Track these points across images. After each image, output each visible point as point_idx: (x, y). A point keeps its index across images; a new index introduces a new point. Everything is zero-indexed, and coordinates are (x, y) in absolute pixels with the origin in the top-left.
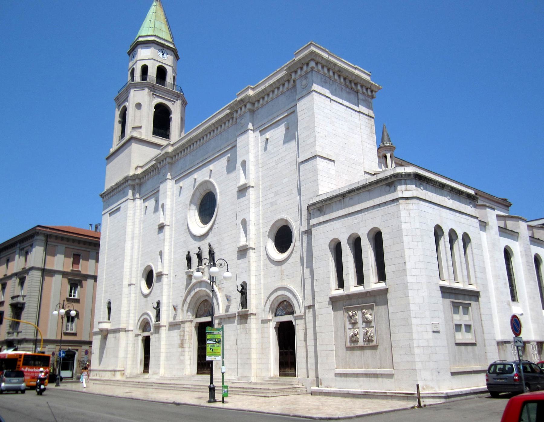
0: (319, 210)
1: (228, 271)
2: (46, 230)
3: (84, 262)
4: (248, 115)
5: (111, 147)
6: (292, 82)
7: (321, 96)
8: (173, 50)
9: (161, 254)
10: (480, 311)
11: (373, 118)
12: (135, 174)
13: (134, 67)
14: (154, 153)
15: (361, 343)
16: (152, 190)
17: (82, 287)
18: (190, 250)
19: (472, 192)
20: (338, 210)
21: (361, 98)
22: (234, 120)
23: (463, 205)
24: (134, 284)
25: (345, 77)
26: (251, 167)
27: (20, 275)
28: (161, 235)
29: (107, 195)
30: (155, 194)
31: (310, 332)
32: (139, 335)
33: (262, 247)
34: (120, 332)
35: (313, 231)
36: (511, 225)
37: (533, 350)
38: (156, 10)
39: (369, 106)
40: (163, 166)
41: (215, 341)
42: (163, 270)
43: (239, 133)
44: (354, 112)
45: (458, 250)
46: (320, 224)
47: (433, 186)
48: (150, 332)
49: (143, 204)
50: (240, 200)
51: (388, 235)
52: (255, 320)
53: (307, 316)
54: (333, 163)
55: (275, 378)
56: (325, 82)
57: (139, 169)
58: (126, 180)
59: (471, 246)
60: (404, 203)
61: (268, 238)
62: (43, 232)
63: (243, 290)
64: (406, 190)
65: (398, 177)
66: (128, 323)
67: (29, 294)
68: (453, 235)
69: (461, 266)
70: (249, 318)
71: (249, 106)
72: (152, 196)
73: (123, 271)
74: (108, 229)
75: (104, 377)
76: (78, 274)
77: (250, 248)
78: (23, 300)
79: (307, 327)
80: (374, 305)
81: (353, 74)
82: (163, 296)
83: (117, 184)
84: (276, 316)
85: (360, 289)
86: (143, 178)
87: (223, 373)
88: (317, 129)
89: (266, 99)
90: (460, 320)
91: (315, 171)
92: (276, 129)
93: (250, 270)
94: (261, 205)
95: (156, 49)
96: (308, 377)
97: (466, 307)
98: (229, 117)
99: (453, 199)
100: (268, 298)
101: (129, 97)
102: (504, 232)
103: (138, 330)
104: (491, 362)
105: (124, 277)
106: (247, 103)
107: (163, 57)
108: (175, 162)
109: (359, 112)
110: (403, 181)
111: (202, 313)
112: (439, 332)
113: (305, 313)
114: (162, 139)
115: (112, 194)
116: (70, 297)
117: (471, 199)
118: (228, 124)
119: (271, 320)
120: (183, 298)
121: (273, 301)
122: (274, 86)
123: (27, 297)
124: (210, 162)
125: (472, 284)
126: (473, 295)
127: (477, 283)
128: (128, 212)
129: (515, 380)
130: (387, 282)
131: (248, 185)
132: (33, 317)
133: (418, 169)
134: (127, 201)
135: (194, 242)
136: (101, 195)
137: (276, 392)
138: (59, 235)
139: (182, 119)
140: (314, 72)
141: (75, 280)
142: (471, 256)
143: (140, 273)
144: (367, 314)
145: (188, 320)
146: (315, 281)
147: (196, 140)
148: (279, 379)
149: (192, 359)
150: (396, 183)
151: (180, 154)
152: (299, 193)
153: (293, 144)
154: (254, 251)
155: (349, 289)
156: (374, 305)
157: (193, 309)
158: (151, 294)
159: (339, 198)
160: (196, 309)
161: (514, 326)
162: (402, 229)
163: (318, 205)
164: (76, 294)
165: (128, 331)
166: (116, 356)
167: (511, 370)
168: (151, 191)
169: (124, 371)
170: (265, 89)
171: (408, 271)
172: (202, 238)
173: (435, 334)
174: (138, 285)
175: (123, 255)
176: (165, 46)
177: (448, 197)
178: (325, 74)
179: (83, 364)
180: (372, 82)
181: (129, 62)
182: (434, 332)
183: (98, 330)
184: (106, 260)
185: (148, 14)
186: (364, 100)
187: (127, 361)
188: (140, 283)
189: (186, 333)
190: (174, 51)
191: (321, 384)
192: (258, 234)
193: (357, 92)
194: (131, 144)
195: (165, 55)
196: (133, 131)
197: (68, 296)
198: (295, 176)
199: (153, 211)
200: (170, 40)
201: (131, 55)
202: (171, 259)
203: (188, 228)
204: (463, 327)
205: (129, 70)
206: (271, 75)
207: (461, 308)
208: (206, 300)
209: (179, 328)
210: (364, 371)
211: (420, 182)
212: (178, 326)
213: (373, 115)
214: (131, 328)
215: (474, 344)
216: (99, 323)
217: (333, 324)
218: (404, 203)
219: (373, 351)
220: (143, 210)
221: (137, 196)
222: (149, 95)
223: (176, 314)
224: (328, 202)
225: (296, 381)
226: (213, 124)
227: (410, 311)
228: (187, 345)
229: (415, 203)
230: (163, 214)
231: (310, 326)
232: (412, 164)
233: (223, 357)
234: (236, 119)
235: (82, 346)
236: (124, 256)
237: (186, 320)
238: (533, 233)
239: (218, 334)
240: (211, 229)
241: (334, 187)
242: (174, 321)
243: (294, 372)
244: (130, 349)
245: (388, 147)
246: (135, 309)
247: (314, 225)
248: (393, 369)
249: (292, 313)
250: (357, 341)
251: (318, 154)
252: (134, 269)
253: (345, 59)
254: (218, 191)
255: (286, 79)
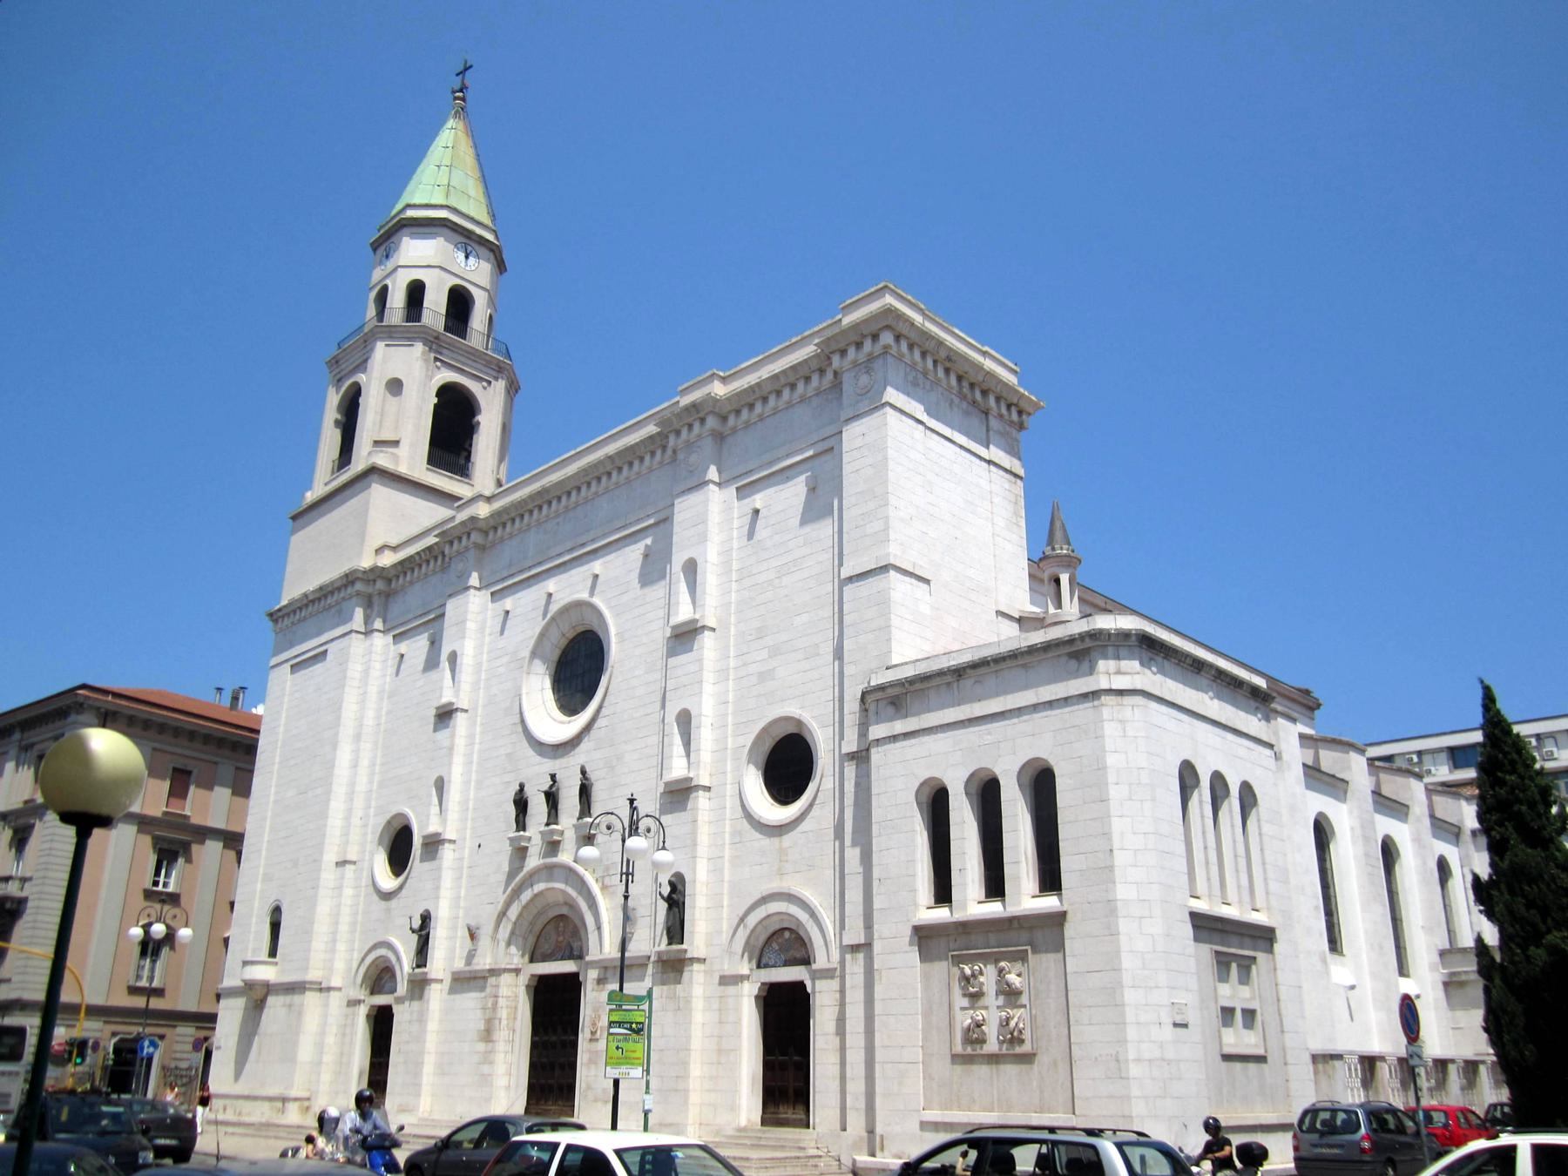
0: (893, 703)
1: (664, 848)
2: (105, 698)
3: (202, 792)
4: (708, 445)
5: (309, 487)
6: (829, 376)
7: (904, 418)
8: (494, 248)
9: (440, 785)
10: (1275, 977)
11: (1021, 478)
12: (377, 567)
13: (388, 282)
14: (430, 514)
15: (992, 1046)
16: (420, 613)
17: (189, 860)
18: (523, 781)
19: (1260, 682)
20: (942, 707)
21: (995, 428)
22: (669, 452)
23: (1242, 714)
24: (354, 863)
25: (960, 373)
26: (710, 579)
27: (17, 818)
28: (443, 735)
29: (288, 615)
30: (433, 622)
31: (855, 1013)
32: (359, 1002)
33: (729, 787)
34: (308, 993)
35: (876, 755)
36: (1329, 760)
37: (1351, 1076)
38: (455, 141)
39: (1013, 448)
40: (459, 553)
41: (631, 1029)
42: (444, 830)
43: (682, 487)
44: (978, 461)
45: (1229, 824)
46: (894, 738)
47: (1178, 664)
48: (396, 994)
49: (392, 648)
50: (673, 661)
51: (1070, 778)
52: (702, 974)
53: (847, 971)
54: (924, 586)
55: (752, 1130)
56: (915, 384)
57: (387, 552)
58: (350, 579)
59: (1258, 815)
60: (1111, 703)
61: (749, 763)
62: (98, 704)
63: (674, 896)
64: (1119, 672)
65: (1100, 640)
66: (330, 969)
67: (41, 874)
68: (1219, 784)
69: (1236, 863)
70: (686, 969)
71: (711, 422)
72: (421, 629)
73: (325, 825)
74: (285, 707)
75: (249, 1114)
76: (181, 823)
77: (697, 787)
78: (22, 889)
79: (847, 1000)
80: (1030, 952)
81: (979, 368)
82: (441, 900)
83: (321, 588)
84: (759, 967)
85: (994, 909)
86: (398, 577)
87: (646, 1113)
88: (892, 500)
89: (758, 408)
90: (1232, 997)
91: (883, 603)
92: (781, 487)
93: (695, 845)
94: (731, 677)
95: (449, 242)
96: (844, 1129)
97: (1246, 965)
98: (655, 444)
99: (1219, 697)
100: (742, 920)
101: (369, 361)
102: (1315, 778)
103: (358, 987)
104: (1306, 1103)
105: (327, 841)
106: (707, 414)
107: (466, 265)
108: (493, 545)
109: (989, 462)
110: (1110, 650)
111: (550, 951)
112: (1185, 1026)
113: (842, 962)
114: (451, 478)
115: (303, 614)
116: (155, 889)
117: (1259, 699)
118: (651, 462)
119: (747, 977)
120: (499, 907)
121: (755, 927)
122: (783, 381)
123: (34, 882)
124: (595, 553)
125: (1198, 895)
126: (1260, 937)
127: (1269, 909)
128: (350, 665)
129: (1363, 1151)
130: (1064, 896)
131: (700, 624)
132: (45, 938)
133: (1146, 622)
134: (347, 637)
135: (538, 758)
136: (271, 615)
137: (766, 1168)
138: (169, 722)
139: (505, 429)
140: (890, 359)
141: (171, 841)
142: (1258, 839)
143: (373, 833)
144: (1010, 972)
145: (508, 967)
146: (875, 883)
147: (558, 493)
148: (764, 1132)
149: (514, 1072)
150: (1094, 654)
151: (509, 526)
152: (839, 654)
153: (824, 530)
154: (707, 794)
155: (964, 907)
156: (1030, 952)
157: (525, 939)
158: (404, 891)
159: (949, 679)
160: (531, 940)
161: (1407, 1021)
162: (1105, 768)
163: (890, 692)
164: (172, 880)
165: (329, 989)
166: (289, 1057)
167: (1351, 1125)
168: (421, 615)
169: (308, 1099)
170: (758, 385)
171: (1117, 872)
172: (560, 751)
173: (1179, 1030)
174: (366, 864)
175: (327, 780)
176: (474, 237)
177: (1211, 694)
178: (903, 356)
179: (176, 1076)
180: (1022, 390)
181: (374, 268)
182: (1176, 1025)
183: (242, 984)
184: (273, 790)
185: (431, 149)
186: (999, 433)
187: (319, 1074)
188: (371, 860)
189: (502, 1002)
190: (497, 252)
191: (882, 1149)
192: (721, 750)
193: (986, 413)
194: (369, 486)
195: (472, 260)
196: (377, 451)
197: (148, 885)
198: (827, 612)
199: (421, 667)
200: (486, 220)
201: (381, 251)
202: (467, 801)
203: (523, 721)
204: (1238, 1014)
205: (371, 289)
206: (774, 350)
207: (1234, 966)
208: (562, 917)
209: (483, 989)
210: (999, 1117)
211: (1150, 654)
212: (481, 982)
213: (1021, 472)
214: (335, 982)
215: (1261, 1059)
216: (245, 963)
217: (920, 996)
218: (1111, 703)
219: (1024, 1067)
220: (390, 663)
221: (378, 624)
222: (426, 360)
223: (475, 950)
224: (918, 686)
225: (811, 1140)
226: (610, 458)
227: (1120, 970)
228: (501, 1035)
229: (1138, 706)
230: (453, 679)
231: (855, 996)
232: (1125, 609)
233: (648, 1071)
234: (674, 452)
235: (175, 1026)
236: (331, 784)
237: (503, 966)
238: (1378, 784)
239: (638, 1010)
240: (588, 728)
241: (927, 649)
242: (467, 968)
243: (803, 1117)
244: (331, 1040)
245: (1065, 559)
246: (353, 932)
247: (878, 740)
248: (1074, 1113)
249: (806, 961)
250: (982, 1041)
251: (892, 562)
252: (356, 821)
253: (961, 330)
254: (613, 630)
255: (814, 365)
